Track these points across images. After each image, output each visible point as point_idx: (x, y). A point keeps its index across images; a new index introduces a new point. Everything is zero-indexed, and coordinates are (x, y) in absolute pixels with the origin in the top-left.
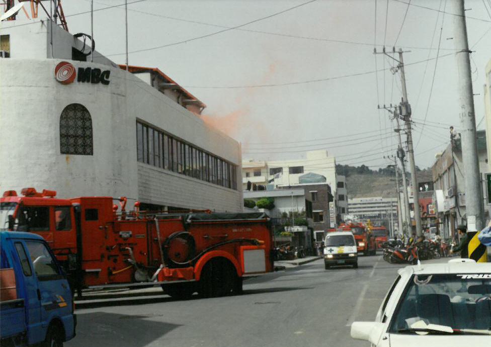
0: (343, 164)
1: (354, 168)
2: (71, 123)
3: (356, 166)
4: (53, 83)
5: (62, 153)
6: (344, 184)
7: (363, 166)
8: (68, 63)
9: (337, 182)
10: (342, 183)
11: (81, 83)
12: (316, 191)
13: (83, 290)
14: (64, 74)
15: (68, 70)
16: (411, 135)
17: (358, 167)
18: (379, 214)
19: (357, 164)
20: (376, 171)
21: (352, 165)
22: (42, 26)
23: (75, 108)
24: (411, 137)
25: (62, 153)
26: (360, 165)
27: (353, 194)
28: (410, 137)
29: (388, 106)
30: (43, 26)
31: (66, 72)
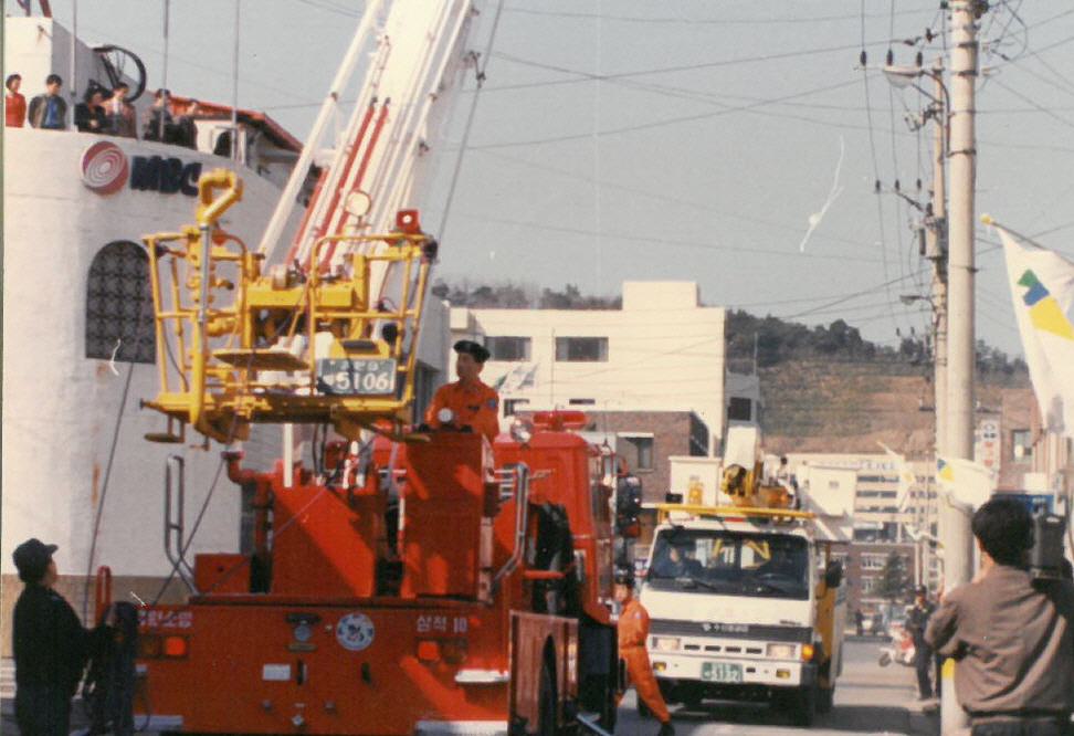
0: (759, 312)
1: (801, 331)
2: (111, 285)
3: (811, 323)
4: (75, 189)
5: (89, 355)
6: (754, 405)
7: (839, 326)
8: (111, 145)
9: (729, 396)
10: (748, 402)
11: (138, 191)
12: (650, 435)
13: (917, 582)
14: (104, 171)
15: (111, 162)
16: (946, 315)
17: (820, 328)
18: (887, 525)
19: (817, 319)
20: (889, 349)
21: (795, 321)
22: (40, 37)
23: (121, 250)
24: (946, 324)
25: (89, 355)
26: (826, 321)
27: (792, 435)
28: (942, 320)
29: (908, 186)
30: (44, 36)
31: (106, 166)
